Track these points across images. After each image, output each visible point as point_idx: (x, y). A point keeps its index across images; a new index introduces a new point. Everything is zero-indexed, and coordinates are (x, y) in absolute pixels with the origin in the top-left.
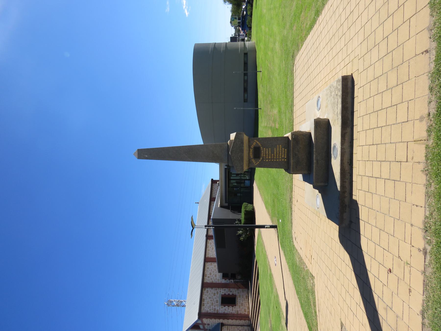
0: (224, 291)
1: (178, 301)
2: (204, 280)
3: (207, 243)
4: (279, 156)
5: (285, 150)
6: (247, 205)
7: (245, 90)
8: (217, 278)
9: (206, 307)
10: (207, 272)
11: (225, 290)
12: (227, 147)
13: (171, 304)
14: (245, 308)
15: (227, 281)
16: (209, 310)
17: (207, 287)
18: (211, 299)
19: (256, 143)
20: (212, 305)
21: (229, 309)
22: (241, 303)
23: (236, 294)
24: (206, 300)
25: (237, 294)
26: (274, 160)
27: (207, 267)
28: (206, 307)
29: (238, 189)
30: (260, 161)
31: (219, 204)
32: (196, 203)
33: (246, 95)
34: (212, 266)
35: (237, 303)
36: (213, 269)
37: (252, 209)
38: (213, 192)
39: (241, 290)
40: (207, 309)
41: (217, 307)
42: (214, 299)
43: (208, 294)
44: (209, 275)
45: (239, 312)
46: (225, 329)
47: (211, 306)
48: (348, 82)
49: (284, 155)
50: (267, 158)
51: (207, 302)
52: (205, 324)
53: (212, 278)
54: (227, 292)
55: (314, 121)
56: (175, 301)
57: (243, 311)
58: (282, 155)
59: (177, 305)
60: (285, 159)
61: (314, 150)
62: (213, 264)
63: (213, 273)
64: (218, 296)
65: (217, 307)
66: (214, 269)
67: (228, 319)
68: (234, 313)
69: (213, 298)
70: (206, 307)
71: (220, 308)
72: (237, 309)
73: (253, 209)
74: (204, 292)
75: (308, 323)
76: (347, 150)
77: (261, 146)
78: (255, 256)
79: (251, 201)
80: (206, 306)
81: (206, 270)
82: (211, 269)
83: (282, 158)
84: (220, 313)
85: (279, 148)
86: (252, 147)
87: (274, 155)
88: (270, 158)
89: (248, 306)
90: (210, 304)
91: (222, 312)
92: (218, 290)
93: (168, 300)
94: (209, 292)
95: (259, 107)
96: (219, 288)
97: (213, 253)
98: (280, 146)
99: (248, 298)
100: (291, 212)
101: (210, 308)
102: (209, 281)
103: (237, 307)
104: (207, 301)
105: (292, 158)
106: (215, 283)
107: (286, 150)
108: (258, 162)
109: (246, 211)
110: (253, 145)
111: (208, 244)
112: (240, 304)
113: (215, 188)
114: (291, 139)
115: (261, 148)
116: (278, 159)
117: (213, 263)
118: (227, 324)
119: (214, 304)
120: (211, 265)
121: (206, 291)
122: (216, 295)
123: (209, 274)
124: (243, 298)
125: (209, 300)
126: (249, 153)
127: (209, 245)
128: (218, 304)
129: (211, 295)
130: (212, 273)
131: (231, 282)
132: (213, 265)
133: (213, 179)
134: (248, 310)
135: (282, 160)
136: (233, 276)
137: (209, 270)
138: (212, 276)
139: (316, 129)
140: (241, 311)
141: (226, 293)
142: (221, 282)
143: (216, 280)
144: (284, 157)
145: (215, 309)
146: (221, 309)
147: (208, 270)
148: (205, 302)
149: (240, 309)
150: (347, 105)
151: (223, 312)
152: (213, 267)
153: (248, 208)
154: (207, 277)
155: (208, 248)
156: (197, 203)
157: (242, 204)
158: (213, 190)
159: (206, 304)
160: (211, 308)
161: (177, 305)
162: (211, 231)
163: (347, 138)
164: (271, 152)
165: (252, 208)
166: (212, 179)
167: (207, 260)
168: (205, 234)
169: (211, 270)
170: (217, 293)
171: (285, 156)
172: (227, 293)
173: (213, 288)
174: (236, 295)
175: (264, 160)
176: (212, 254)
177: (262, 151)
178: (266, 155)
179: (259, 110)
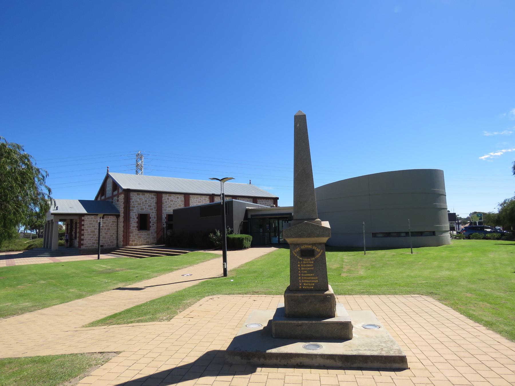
0: (153, 217)
1: (142, 166)
4: (305, 280)
5: (312, 286)
6: (250, 240)
9: (136, 197)
11: (155, 218)
13: (139, 158)
14: (136, 241)
15: (164, 220)
16: (133, 200)
17: (157, 198)
18: (144, 203)
19: (320, 252)
20: (138, 204)
21: (134, 222)
22: (141, 236)
24: (144, 197)
25: (150, 231)
26: (299, 273)
28: (136, 197)
30: (298, 257)
31: (250, 208)
32: (250, 180)
34: (180, 203)
35: (141, 231)
36: (177, 203)
37: (245, 246)
39: (155, 235)
41: (136, 210)
42: (145, 205)
43: (149, 199)
44: (170, 199)
45: (131, 234)
46: (113, 220)
47: (137, 203)
48: (399, 363)
49: (306, 286)
50: (302, 265)
52: (118, 197)
53: (168, 202)
54: (153, 220)
55: (348, 322)
57: (133, 238)
58: (306, 283)
61: (314, 322)
63: (173, 204)
64: (148, 210)
66: (177, 205)
68: (131, 228)
71: (135, 213)
74: (152, 194)
75: (120, 313)
76: (314, 362)
77: (316, 258)
78: (192, 251)
79: (254, 245)
81: (175, 195)
82: (177, 202)
85: (314, 280)
87: (305, 273)
88: (302, 269)
89: (138, 244)
90: (139, 201)
91: (131, 215)
92: (154, 210)
93: (143, 155)
94: (152, 200)
95: (366, 252)
96: (156, 211)
97: (194, 202)
98: (317, 281)
99: (147, 244)
101: (136, 202)
102: (164, 199)
105: (303, 295)
106: (162, 206)
107: (313, 287)
108: (296, 255)
109: (243, 239)
110: (316, 249)
115: (314, 259)
116: (301, 275)
118: (118, 221)
119: (139, 206)
121: (153, 197)
122: (149, 208)
124: (147, 238)
125: (144, 200)
126: (307, 244)
129: (149, 202)
131: (164, 225)
132: (181, 203)
134: (134, 245)
135: (300, 283)
136: (170, 226)
140: (132, 237)
141: (151, 219)
142: (164, 213)
143: (166, 208)
145: (134, 208)
148: (141, 196)
149: (135, 236)
150: (370, 362)
152: (179, 204)
153: (246, 242)
155: (200, 197)
156: (250, 182)
157: (251, 235)
159: (139, 198)
161: (137, 165)
163: (328, 362)
164: (309, 270)
166: (278, 198)
167: (187, 196)
168: (216, 193)
170: (152, 209)
171: (306, 287)
172: (152, 220)
173: (156, 205)
175: (299, 262)
177: (310, 260)
178: (306, 264)
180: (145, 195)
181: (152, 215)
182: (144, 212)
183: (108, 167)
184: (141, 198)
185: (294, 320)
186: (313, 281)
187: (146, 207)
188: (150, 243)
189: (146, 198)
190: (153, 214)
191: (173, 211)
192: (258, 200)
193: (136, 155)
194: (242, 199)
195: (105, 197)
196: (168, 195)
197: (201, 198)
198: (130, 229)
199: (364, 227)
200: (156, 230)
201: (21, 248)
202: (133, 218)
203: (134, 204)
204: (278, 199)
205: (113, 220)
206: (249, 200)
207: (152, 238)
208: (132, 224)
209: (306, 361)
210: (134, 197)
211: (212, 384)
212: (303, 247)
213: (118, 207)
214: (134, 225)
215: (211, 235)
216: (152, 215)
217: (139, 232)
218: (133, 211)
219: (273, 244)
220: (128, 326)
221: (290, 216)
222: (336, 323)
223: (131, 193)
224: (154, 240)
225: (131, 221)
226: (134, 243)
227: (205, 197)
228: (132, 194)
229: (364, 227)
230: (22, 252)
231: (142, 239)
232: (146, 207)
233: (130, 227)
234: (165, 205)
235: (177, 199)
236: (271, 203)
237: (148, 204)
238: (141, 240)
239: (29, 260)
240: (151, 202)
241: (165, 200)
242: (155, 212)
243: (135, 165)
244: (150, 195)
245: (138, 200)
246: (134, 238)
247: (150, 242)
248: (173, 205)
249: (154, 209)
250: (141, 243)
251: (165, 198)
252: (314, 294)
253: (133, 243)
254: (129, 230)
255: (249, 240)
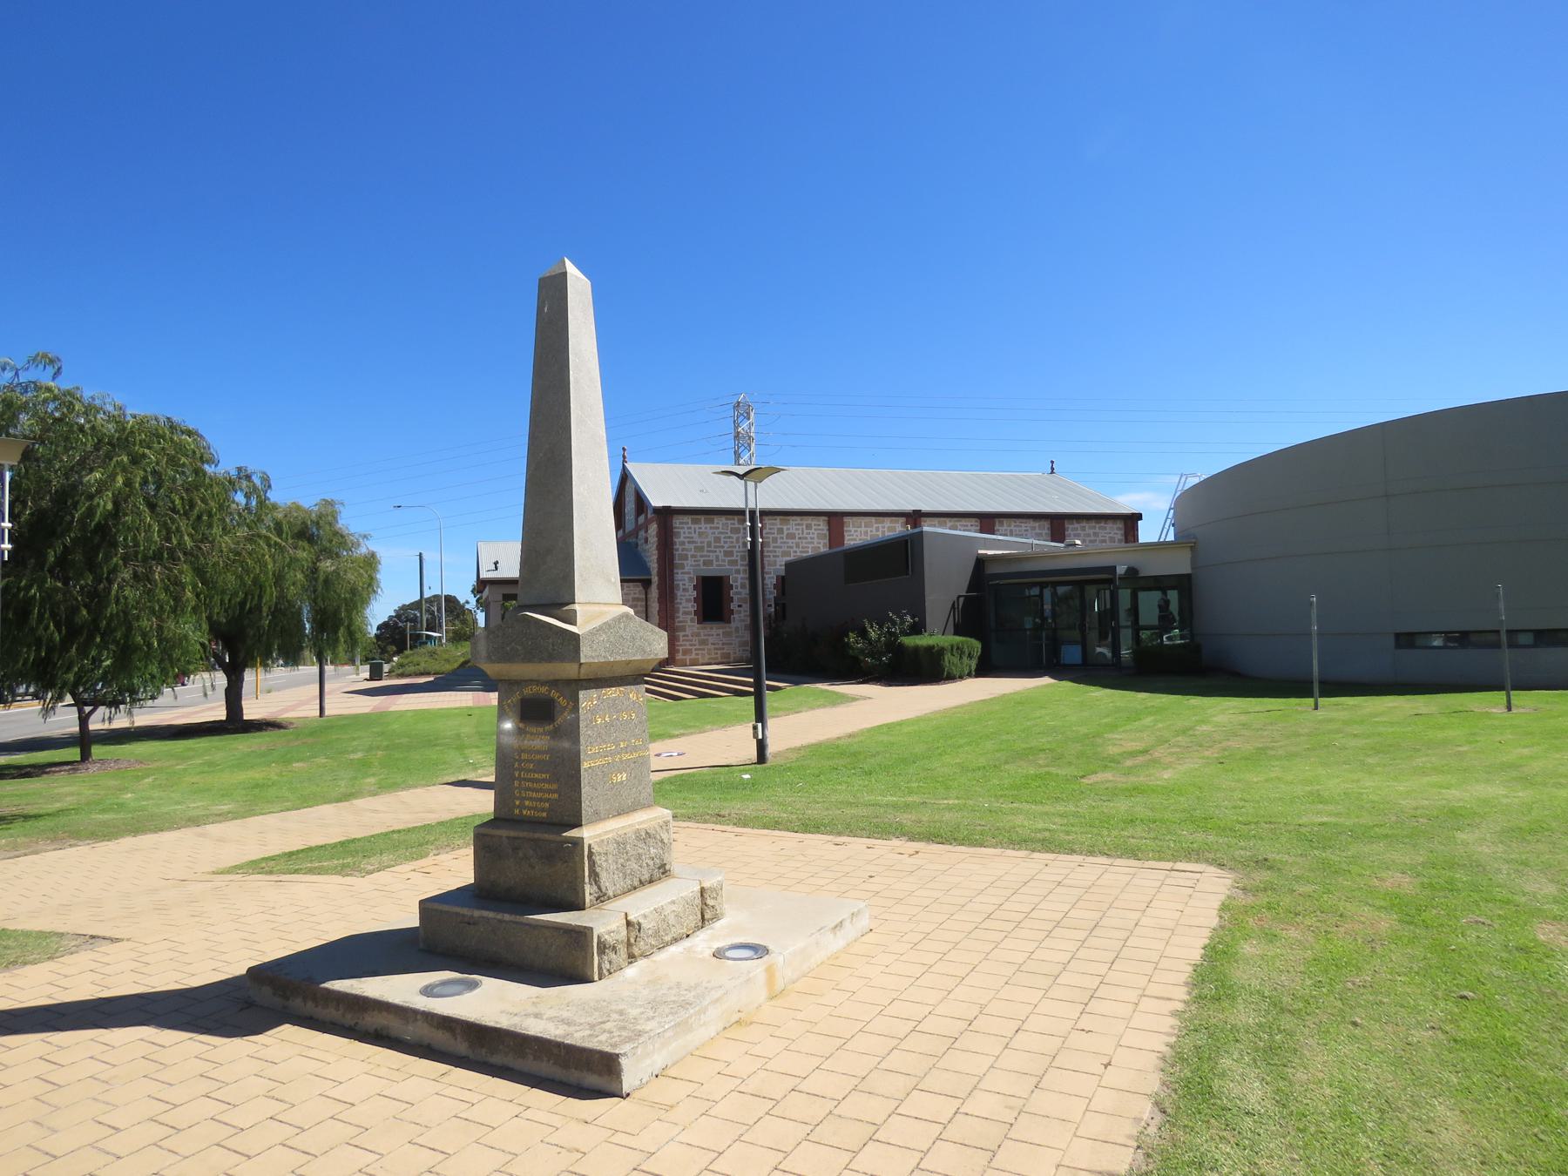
1: (750, 437)
2: (770, 517)
3: (942, 519)
4: (529, 789)
5: (543, 810)
6: (969, 654)
7: (1462, 639)
8: (778, 559)
9: (690, 528)
10: (796, 525)
11: (743, 586)
12: (560, 602)
13: (742, 414)
14: (694, 652)
16: (682, 539)
18: (713, 545)
20: (695, 547)
21: (688, 601)
22: (707, 640)
23: (734, 621)
24: (711, 528)
25: (733, 625)
27: (813, 523)
28: (690, 528)
29: (1050, 621)
31: (990, 552)
32: (1052, 462)
33: (1437, 642)
34: (816, 541)
35: (708, 625)
36: (806, 543)
37: (948, 673)
38: (1087, 525)
40: (684, 531)
41: (691, 565)
44: (785, 532)
45: (681, 634)
46: (635, 594)
47: (692, 546)
48: (600, 1075)
49: (530, 808)
51: (705, 532)
52: (646, 531)
53: (779, 541)
54: (739, 593)
55: (585, 927)
56: (750, 428)
57: (685, 645)
58: (531, 799)
59: (738, 433)
60: (520, 811)
61: (507, 917)
62: (822, 541)
63: (794, 545)
65: (691, 565)
67: (659, 602)
68: (679, 617)
69: (717, 550)
70: (688, 528)
71: (689, 573)
72: (689, 626)
73: (951, 678)
74: (734, 519)
75: (298, 852)
76: (410, 1032)
78: (796, 683)
79: (986, 668)
80: (693, 531)
81: (801, 520)
82: (806, 538)
83: (523, 799)
84: (676, 575)
86: (554, 694)
87: (530, 771)
89: (701, 661)
90: (699, 541)
91: (678, 580)
92: (742, 565)
94: (735, 536)
95: (1322, 701)
96: (747, 568)
97: (857, 535)
100: (682, 815)
101: (689, 542)
103: (693, 626)
104: (708, 530)
105: (512, 834)
107: (544, 814)
109: (942, 651)
111: (888, 520)
112: (705, 635)
113: (1105, 528)
114: (564, 834)
117: (827, 541)
118: (649, 596)
120: (818, 538)
121: (737, 526)
122: (727, 559)
123: (791, 531)
124: (723, 644)
126: (531, 681)
127: (886, 526)
128: (702, 567)
129: (725, 542)
130: (794, 541)
132: (820, 543)
133: (1141, 519)
134: (688, 663)
135: (518, 798)
137: (803, 531)
138: (785, 543)
139: (562, 931)
140: (683, 641)
144: (525, 808)
145: (687, 559)
146: (686, 576)
147: (804, 527)
148: (703, 526)
149: (690, 638)
150: (531, 1057)
151: (678, 585)
152: (814, 542)
153: (955, 660)
154: (781, 524)
155: (876, 523)
156: (1052, 469)
157: (977, 639)
158: (1098, 523)
159: (697, 530)
160: (687, 546)
161: (737, 436)
162: (688, 540)
163: (440, 1038)
164: (539, 762)
165: (956, 672)
166: (1139, 517)
167: (835, 520)
168: (925, 508)
169: (805, 535)
170: (734, 563)
172: (737, 593)
174: (729, 621)
176: (855, 537)
179: (1310, 701)
180: (713, 523)
181: (736, 578)
182: (713, 570)
183: (624, 449)
184: (703, 530)
185: (504, 912)
186: (546, 796)
187: (717, 557)
188: (732, 660)
189: (716, 531)
190: (739, 576)
191: (783, 567)
192: (1066, 526)
193: (734, 407)
194: (936, 521)
195: (624, 531)
196: (778, 521)
197: (880, 525)
198: (677, 620)
199: (1314, 611)
200: (749, 622)
201: (436, 667)
202: (684, 589)
203: (687, 550)
204: (1141, 519)
205: (636, 596)
206: (1037, 524)
207: (737, 644)
208: (681, 606)
209: (394, 1025)
210: (684, 529)
211: (984, 1075)
212: (528, 691)
213: (647, 560)
214: (688, 608)
215: (852, 637)
216: (736, 578)
217: (702, 629)
218: (683, 568)
219: (1065, 665)
220: (244, 879)
221: (1110, 576)
222: (553, 928)
223: (675, 517)
224: (744, 650)
225: (679, 598)
226: (690, 659)
227: (891, 522)
228: (678, 521)
229: (1314, 611)
230: (431, 679)
231: (710, 646)
232: (717, 557)
233: (677, 615)
234: (771, 549)
235: (805, 531)
236: (1116, 531)
237: (723, 547)
238: (709, 650)
239: (435, 699)
240: (732, 542)
241: (771, 536)
242: (745, 570)
243: (732, 436)
244: (729, 522)
245: (696, 537)
246: (688, 643)
247: (732, 656)
248: (795, 549)
249: (741, 560)
250: (709, 659)
251: (770, 529)
252: (537, 835)
253: (686, 659)
254: (674, 624)
255: (967, 653)
